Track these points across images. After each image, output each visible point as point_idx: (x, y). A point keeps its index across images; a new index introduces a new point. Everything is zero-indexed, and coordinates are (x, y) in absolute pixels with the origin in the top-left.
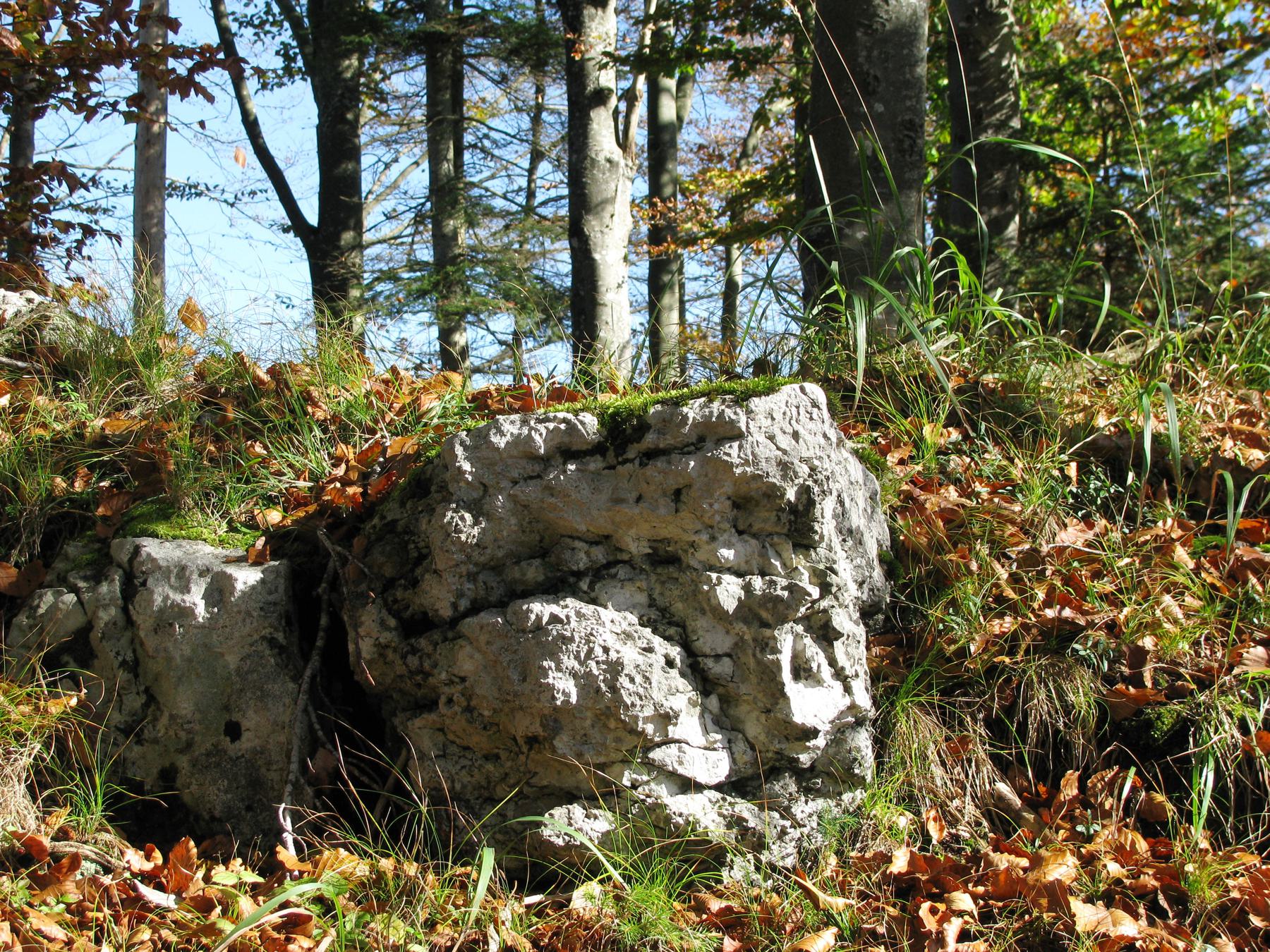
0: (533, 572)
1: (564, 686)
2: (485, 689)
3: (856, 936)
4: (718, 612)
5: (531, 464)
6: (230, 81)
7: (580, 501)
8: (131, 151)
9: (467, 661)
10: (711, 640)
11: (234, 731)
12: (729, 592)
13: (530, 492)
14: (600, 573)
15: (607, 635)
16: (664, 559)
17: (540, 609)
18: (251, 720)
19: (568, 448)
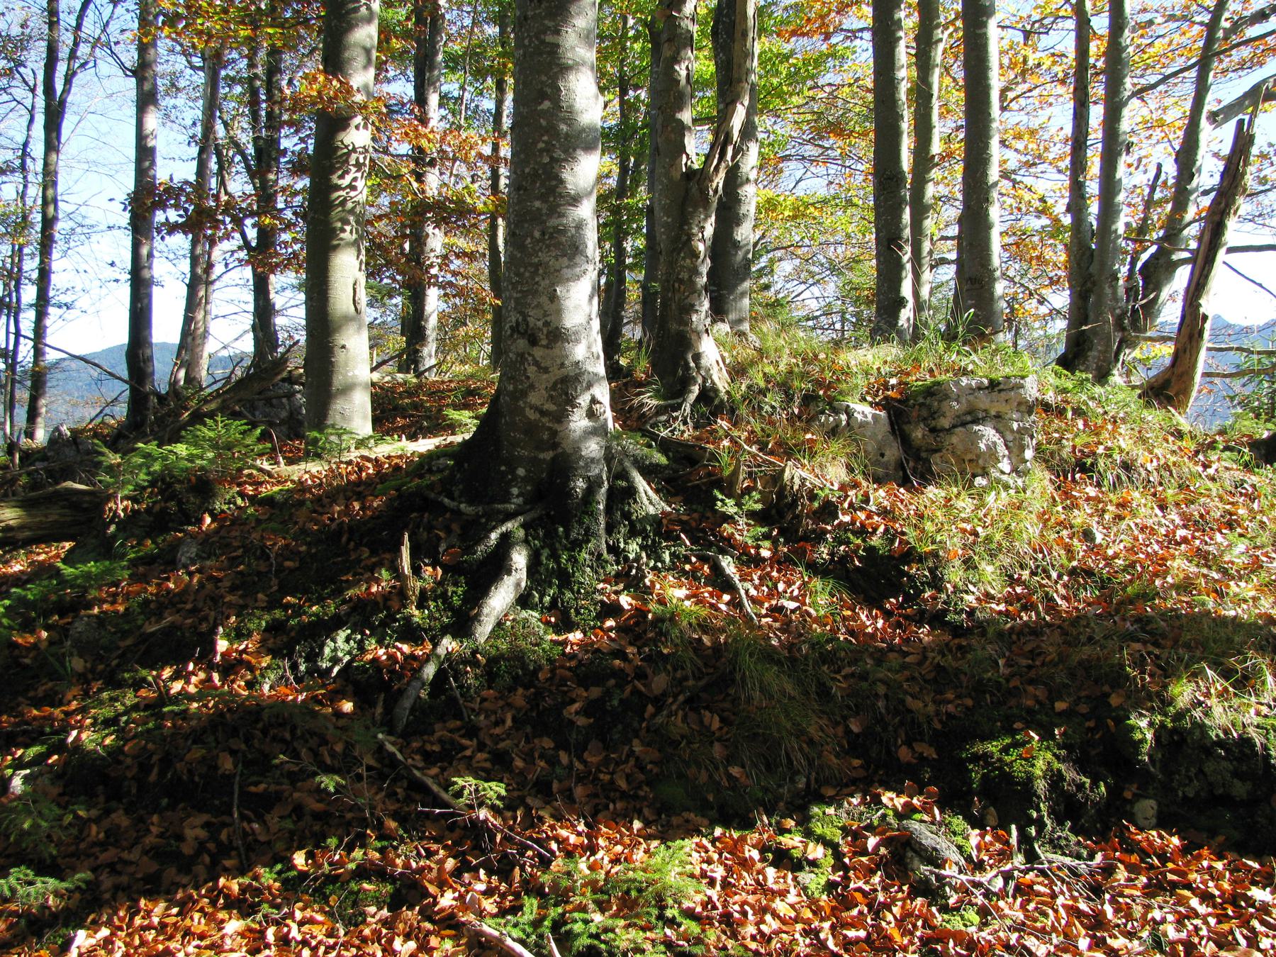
0: (969, 418)
1: (982, 446)
2: (960, 447)
3: (5, 467)
4: (1012, 431)
5: (972, 391)
6: (596, 324)
7: (983, 401)
8: (250, 337)
9: (954, 440)
10: (1010, 437)
11: (882, 455)
12: (1015, 426)
13: (971, 398)
14: (984, 419)
15: (988, 434)
16: (998, 416)
17: (976, 428)
18: (887, 453)
19: (980, 388)
